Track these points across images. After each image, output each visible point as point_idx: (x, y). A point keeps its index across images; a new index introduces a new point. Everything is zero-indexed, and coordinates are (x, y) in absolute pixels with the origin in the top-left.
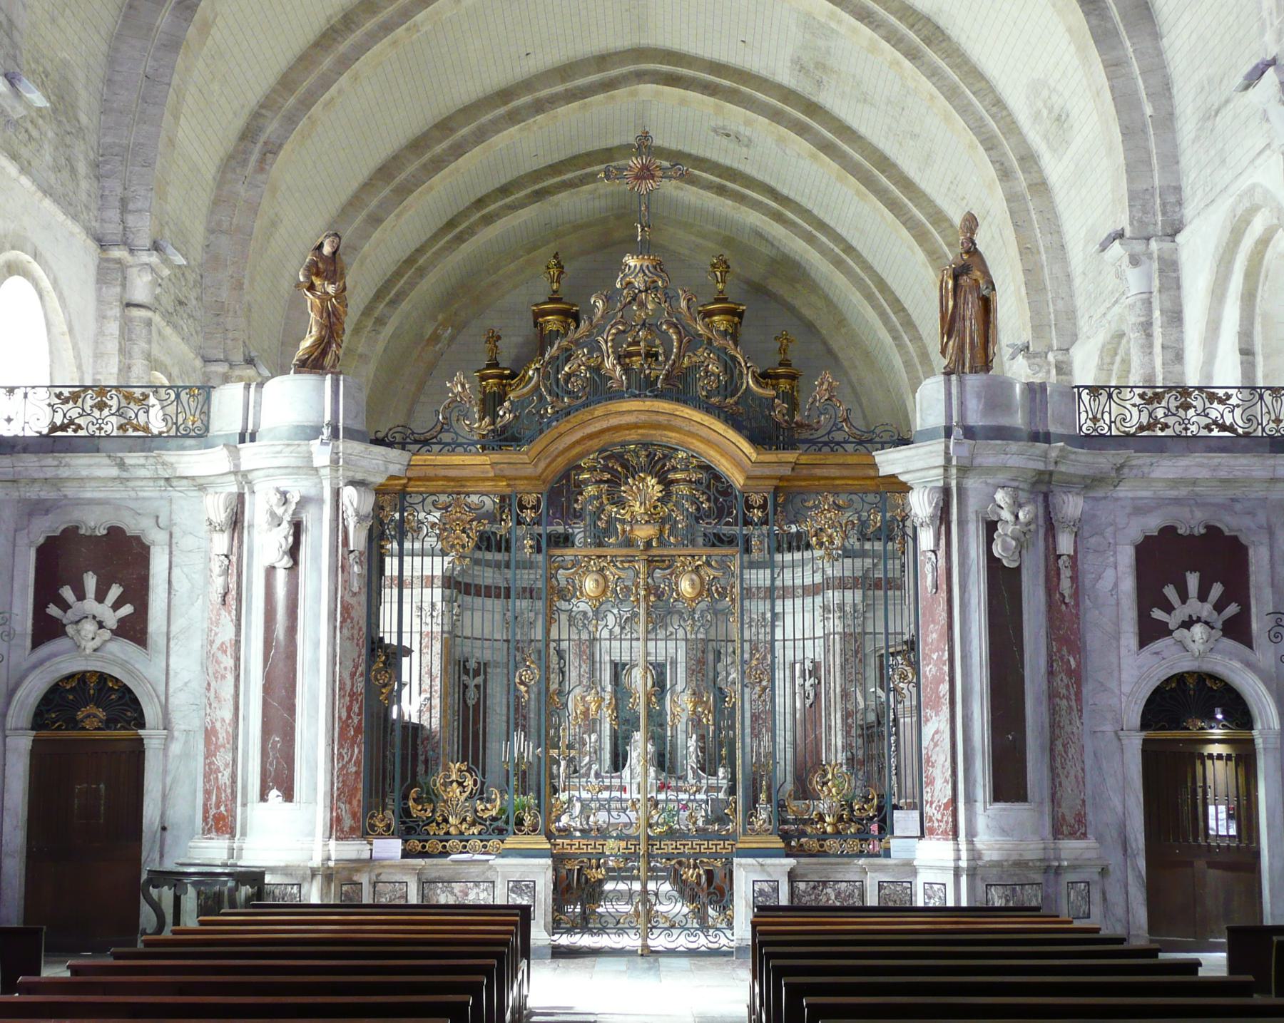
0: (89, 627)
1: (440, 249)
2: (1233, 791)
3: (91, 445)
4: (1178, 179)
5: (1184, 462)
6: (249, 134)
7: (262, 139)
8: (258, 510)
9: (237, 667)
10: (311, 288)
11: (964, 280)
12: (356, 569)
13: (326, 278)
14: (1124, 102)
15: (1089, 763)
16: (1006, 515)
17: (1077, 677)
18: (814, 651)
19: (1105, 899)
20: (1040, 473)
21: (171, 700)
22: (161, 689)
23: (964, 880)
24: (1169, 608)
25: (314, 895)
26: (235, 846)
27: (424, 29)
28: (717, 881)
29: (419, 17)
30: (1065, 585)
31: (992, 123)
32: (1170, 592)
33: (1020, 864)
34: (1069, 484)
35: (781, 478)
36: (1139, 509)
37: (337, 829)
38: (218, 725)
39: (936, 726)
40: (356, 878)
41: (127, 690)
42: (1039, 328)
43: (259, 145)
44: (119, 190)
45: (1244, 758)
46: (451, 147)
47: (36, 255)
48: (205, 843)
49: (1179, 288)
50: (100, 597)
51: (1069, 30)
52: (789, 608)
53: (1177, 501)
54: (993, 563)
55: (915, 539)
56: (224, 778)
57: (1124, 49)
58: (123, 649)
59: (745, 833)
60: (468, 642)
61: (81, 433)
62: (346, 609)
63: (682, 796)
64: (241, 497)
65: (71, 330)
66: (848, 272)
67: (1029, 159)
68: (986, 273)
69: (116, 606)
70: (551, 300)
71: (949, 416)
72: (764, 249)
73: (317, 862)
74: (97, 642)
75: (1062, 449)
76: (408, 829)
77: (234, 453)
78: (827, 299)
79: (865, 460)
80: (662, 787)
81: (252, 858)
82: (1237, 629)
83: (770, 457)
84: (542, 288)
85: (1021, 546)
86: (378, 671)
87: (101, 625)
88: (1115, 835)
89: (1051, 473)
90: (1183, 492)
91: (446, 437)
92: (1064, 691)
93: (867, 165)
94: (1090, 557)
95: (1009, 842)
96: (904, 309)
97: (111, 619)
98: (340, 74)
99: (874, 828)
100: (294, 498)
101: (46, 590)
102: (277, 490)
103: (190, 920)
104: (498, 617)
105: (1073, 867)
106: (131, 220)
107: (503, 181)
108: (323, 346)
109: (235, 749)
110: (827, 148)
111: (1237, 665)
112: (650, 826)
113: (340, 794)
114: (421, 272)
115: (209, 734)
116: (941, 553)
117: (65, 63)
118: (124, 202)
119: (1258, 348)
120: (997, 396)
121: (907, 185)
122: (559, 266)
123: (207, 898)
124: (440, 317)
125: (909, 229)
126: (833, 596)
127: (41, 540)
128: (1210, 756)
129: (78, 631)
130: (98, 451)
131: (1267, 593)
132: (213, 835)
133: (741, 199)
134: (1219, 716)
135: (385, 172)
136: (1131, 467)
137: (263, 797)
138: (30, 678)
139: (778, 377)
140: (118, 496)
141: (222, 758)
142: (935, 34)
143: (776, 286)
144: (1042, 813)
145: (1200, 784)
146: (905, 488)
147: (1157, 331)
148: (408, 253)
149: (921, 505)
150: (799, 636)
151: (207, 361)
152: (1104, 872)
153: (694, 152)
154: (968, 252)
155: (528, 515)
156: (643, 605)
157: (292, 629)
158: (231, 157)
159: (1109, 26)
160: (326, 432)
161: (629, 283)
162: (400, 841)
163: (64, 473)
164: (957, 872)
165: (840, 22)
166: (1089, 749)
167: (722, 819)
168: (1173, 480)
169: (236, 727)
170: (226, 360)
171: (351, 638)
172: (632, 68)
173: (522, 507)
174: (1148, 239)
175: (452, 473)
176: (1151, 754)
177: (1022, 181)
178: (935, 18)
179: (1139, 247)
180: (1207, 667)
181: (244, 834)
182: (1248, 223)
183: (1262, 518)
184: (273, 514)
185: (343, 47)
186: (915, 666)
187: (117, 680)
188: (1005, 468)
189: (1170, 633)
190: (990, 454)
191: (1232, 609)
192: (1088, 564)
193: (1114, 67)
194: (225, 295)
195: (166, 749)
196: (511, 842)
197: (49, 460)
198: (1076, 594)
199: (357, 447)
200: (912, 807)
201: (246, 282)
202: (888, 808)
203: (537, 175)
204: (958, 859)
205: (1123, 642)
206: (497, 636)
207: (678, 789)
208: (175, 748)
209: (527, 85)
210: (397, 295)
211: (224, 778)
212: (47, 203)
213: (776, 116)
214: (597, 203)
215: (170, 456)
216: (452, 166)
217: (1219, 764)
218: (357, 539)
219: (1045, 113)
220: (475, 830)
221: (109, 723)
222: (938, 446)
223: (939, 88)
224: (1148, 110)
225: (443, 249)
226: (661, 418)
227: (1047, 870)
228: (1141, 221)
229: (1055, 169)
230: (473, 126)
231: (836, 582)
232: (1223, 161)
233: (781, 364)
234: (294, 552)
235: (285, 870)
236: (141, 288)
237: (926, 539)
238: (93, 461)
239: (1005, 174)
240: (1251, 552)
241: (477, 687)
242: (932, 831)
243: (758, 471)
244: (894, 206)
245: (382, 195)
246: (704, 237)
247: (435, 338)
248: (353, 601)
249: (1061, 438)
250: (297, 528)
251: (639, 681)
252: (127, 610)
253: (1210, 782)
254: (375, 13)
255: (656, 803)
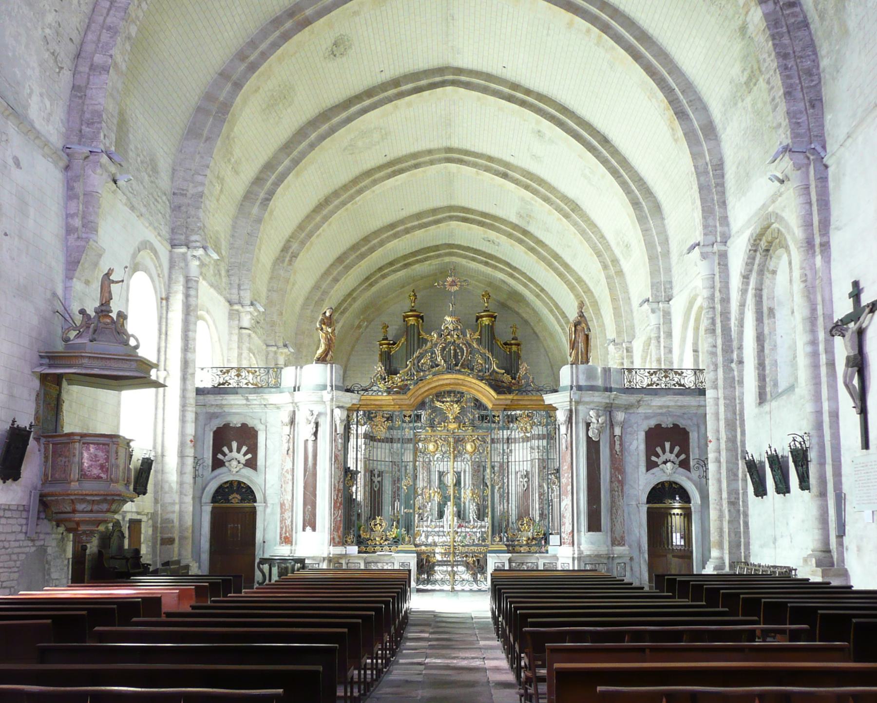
0: (234, 463)
1: (363, 289)
2: (682, 528)
3: (234, 391)
4: (671, 278)
5: (664, 399)
6: (285, 249)
7: (291, 250)
8: (300, 418)
9: (293, 479)
10: (322, 329)
11: (579, 327)
12: (340, 441)
13: (328, 326)
14: (650, 245)
15: (626, 515)
16: (594, 420)
17: (622, 483)
18: (527, 466)
19: (632, 570)
20: (607, 403)
21: (267, 492)
22: (263, 487)
23: (576, 562)
24: (658, 456)
25: (324, 566)
26: (293, 549)
27: (359, 203)
28: (481, 563)
29: (357, 199)
30: (617, 447)
31: (600, 246)
32: (659, 450)
33: (598, 556)
34: (619, 408)
35: (506, 405)
36: (647, 417)
37: (333, 542)
38: (286, 502)
39: (566, 502)
40: (340, 561)
41: (249, 488)
42: (619, 333)
43: (290, 254)
44: (237, 281)
45: (687, 515)
46: (368, 249)
47: (208, 312)
48: (281, 548)
49: (671, 323)
50: (238, 451)
51: (628, 214)
52: (517, 448)
53: (661, 414)
54: (589, 439)
55: (559, 429)
56: (288, 522)
57: (649, 224)
58: (248, 472)
59: (492, 544)
60: (379, 463)
61: (230, 386)
62: (336, 456)
63: (468, 530)
64: (294, 412)
65: (219, 340)
66: (542, 300)
67: (615, 261)
68: (587, 325)
69: (245, 455)
70: (411, 311)
71: (572, 382)
72: (505, 287)
73: (325, 555)
74: (238, 469)
75: (616, 395)
76: (360, 542)
77: (292, 396)
78: (533, 309)
79: (539, 398)
80: (460, 526)
81: (299, 554)
82: (685, 465)
83: (502, 397)
84: (407, 305)
85: (600, 433)
86: (348, 480)
87: (239, 462)
88: (636, 545)
89: (612, 404)
90: (664, 410)
91: (375, 388)
92: (616, 489)
93: (549, 257)
94: (628, 436)
95: (593, 547)
96: (566, 317)
97: (243, 460)
98: (324, 223)
99: (543, 542)
100: (316, 413)
101: (217, 448)
102: (21, 168)
103: (275, 577)
104: (387, 451)
105: (619, 557)
106: (242, 293)
107: (390, 260)
108: (326, 352)
109: (292, 511)
110: (532, 250)
111: (684, 478)
112: (455, 541)
113: (335, 529)
114: (354, 300)
115: (282, 505)
116: (569, 435)
117: (217, 231)
118: (239, 286)
119: (700, 350)
120: (591, 374)
121: (566, 266)
122: (415, 295)
123: (282, 569)
124: (362, 317)
125: (567, 285)
126: (535, 443)
127: (215, 429)
128: (674, 514)
129: (230, 465)
130: (237, 394)
131: (697, 451)
132: (284, 544)
133: (495, 267)
134: (677, 498)
135: (340, 260)
136: (643, 401)
137: (304, 530)
138: (210, 484)
139: (511, 344)
140: (245, 411)
141: (287, 515)
142: (576, 207)
143: (510, 303)
144: (607, 536)
145: (670, 524)
146: (556, 409)
147: (662, 340)
148: (349, 291)
149: (561, 416)
150: (517, 460)
151: (268, 346)
152: (631, 559)
153: (474, 247)
154: (580, 316)
155: (407, 419)
156: (452, 455)
157: (315, 464)
158: (278, 259)
159: (644, 214)
160: (329, 388)
161: (447, 327)
162: (357, 547)
163: (224, 402)
164: (573, 559)
165: (536, 201)
166: (626, 511)
167: (484, 540)
168: (660, 406)
169: (293, 503)
170: (276, 346)
171: (338, 468)
172: (448, 214)
173: (405, 416)
174: (659, 302)
175: (377, 403)
176: (650, 513)
177: (612, 270)
178: (576, 201)
179: (655, 305)
180: (672, 479)
181: (296, 544)
182: (696, 300)
183: (695, 420)
184: (307, 419)
185: (325, 212)
186: (559, 478)
187: (245, 484)
188: (593, 402)
189: (658, 466)
190: (588, 397)
191: (683, 456)
192: (627, 439)
193: (645, 231)
194: (275, 317)
195: (265, 511)
196: (400, 547)
197: (219, 397)
198: (621, 451)
199: (340, 393)
200: (557, 534)
201: (284, 312)
202: (547, 535)
203: (405, 257)
204: (574, 554)
205: (640, 470)
206: (387, 460)
207: (466, 527)
208: (268, 510)
209: (402, 222)
210: (344, 310)
211: (288, 522)
212: (212, 290)
213: (510, 236)
214: (432, 267)
215: (266, 396)
216: (369, 257)
217: (678, 517)
218: (340, 429)
219: (621, 243)
220: (386, 543)
221: (242, 500)
222: (567, 393)
223: (578, 231)
224: (659, 250)
225: (364, 289)
226: (459, 381)
227: (609, 558)
228: (656, 295)
229: (625, 266)
230: (379, 239)
231: (536, 436)
232: (686, 274)
233: (513, 339)
234: (315, 434)
235: (313, 558)
236: (246, 321)
237: (563, 429)
238: (236, 398)
239: (605, 267)
240: (690, 434)
241: (378, 482)
242: (564, 543)
243: (498, 402)
244: (560, 275)
245: (339, 269)
246: (479, 282)
247: (359, 326)
248: (339, 453)
249: (618, 390)
250: (317, 424)
251: (450, 480)
252: (249, 456)
253: (674, 524)
254: (338, 198)
255: (457, 533)
